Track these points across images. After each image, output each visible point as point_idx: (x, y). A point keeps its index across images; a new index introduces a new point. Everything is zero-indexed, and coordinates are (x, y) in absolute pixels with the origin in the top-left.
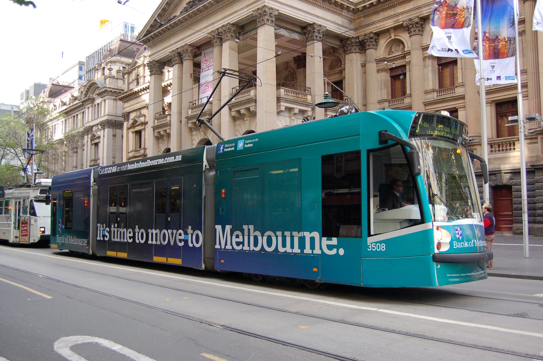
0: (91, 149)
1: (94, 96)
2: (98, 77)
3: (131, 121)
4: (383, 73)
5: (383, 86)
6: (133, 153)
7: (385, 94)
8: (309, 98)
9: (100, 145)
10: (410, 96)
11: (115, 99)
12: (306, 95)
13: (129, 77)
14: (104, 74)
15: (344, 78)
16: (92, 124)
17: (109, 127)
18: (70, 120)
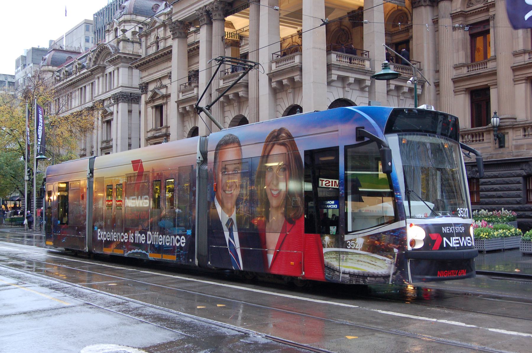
0: (102, 128)
1: (105, 63)
2: (109, 39)
3: (150, 94)
5: (460, 46)
6: (153, 133)
7: (461, 57)
8: (367, 64)
9: (113, 123)
10: (495, 59)
12: (363, 60)
13: (147, 40)
15: (412, 37)
16: (103, 97)
17: (123, 102)
18: (77, 93)
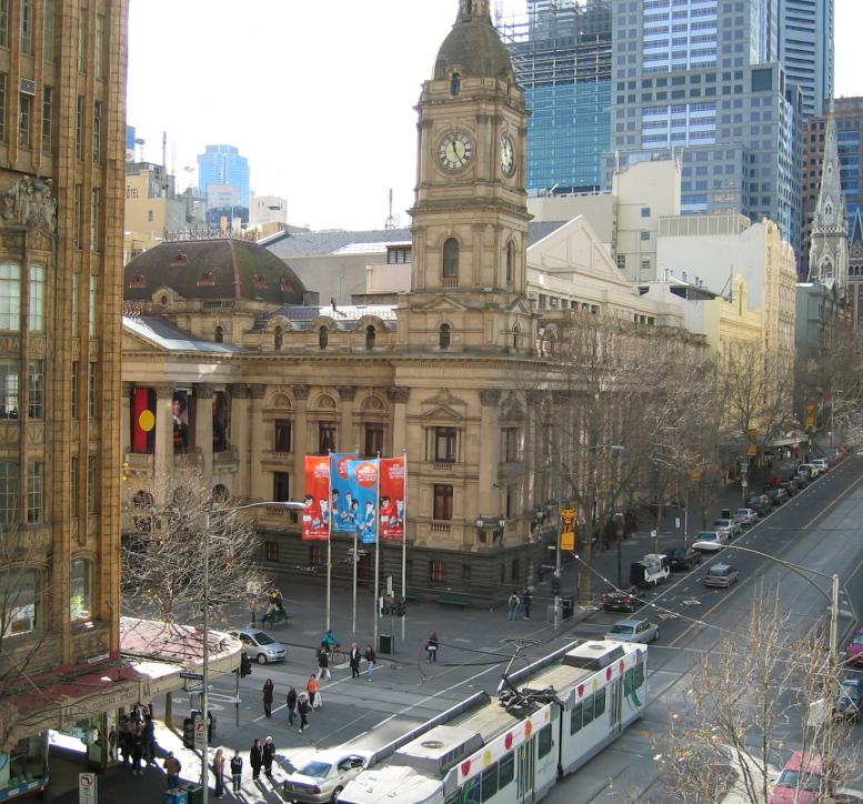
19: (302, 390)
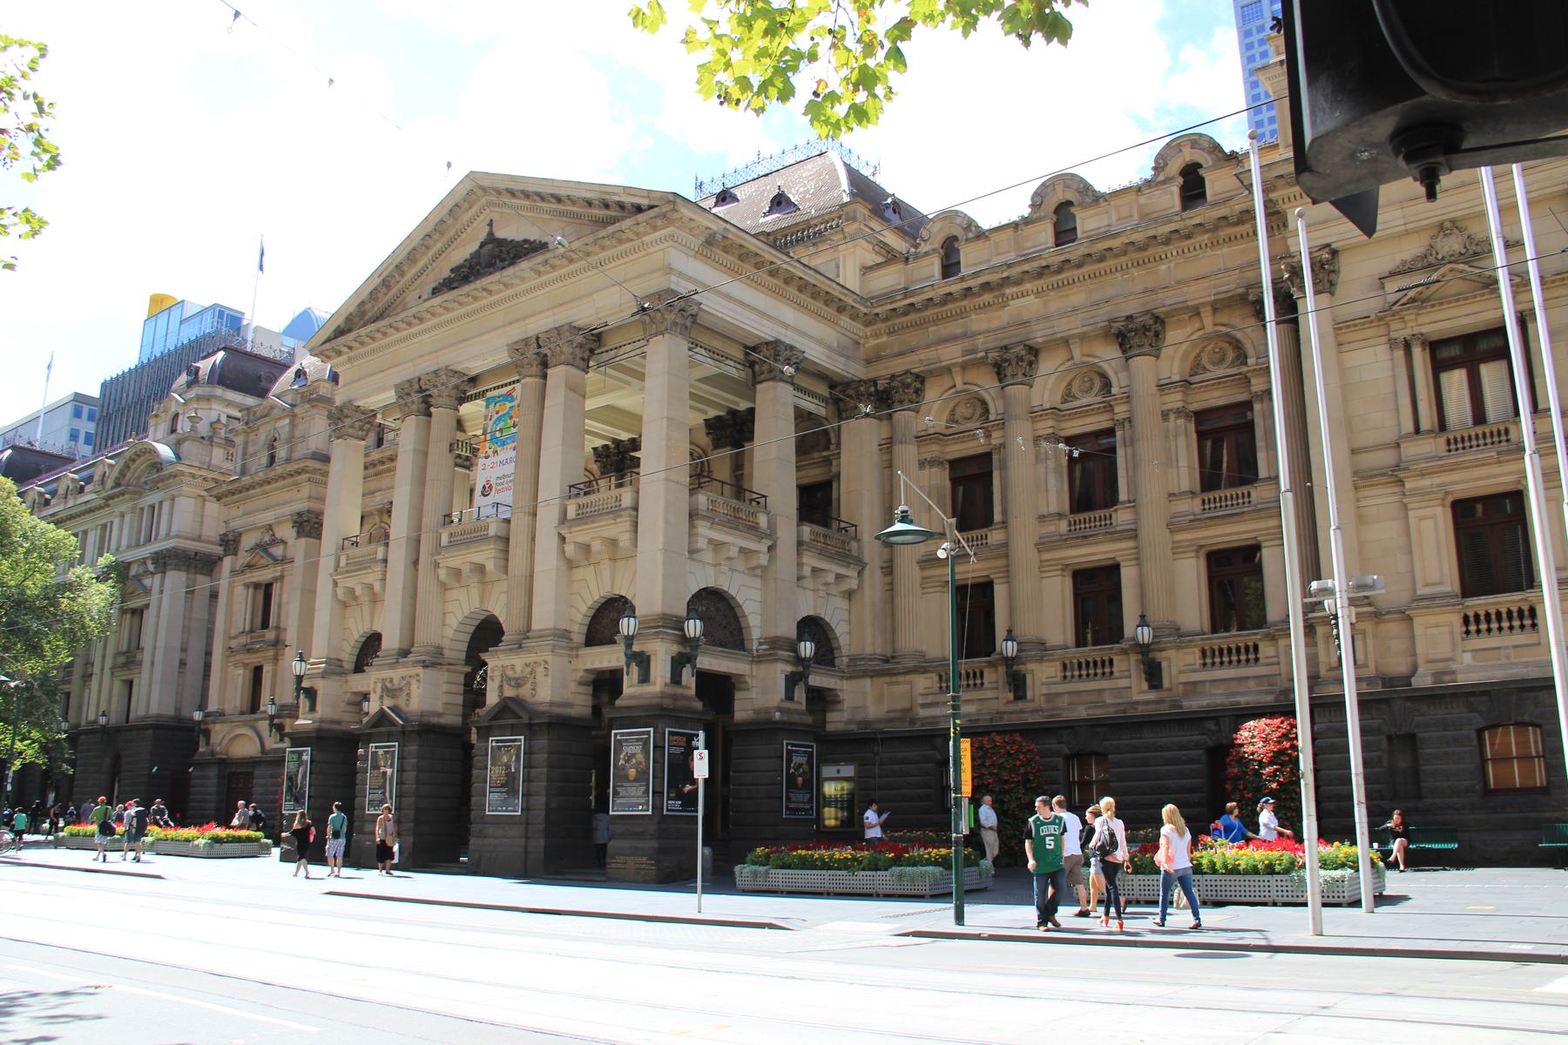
4: (935, 470)
9: (150, 616)
10: (1133, 503)
11: (913, 293)
14: (173, 431)
15: (838, 475)
19: (1016, 360)
